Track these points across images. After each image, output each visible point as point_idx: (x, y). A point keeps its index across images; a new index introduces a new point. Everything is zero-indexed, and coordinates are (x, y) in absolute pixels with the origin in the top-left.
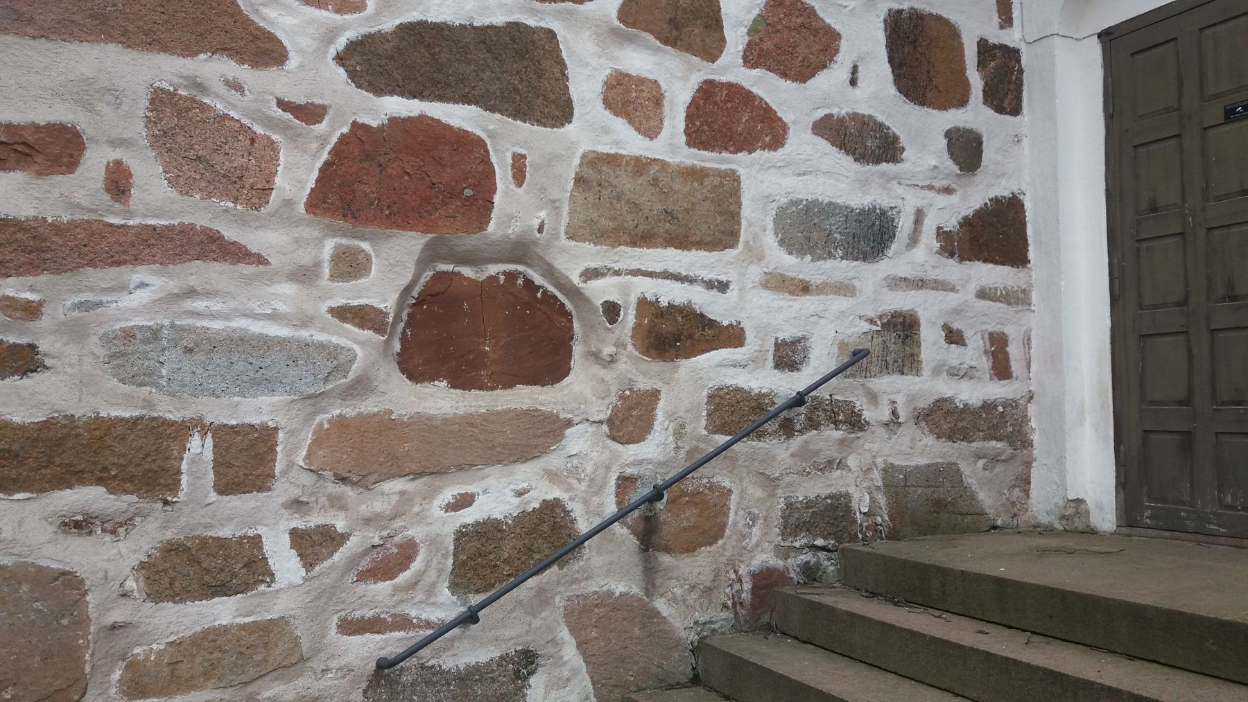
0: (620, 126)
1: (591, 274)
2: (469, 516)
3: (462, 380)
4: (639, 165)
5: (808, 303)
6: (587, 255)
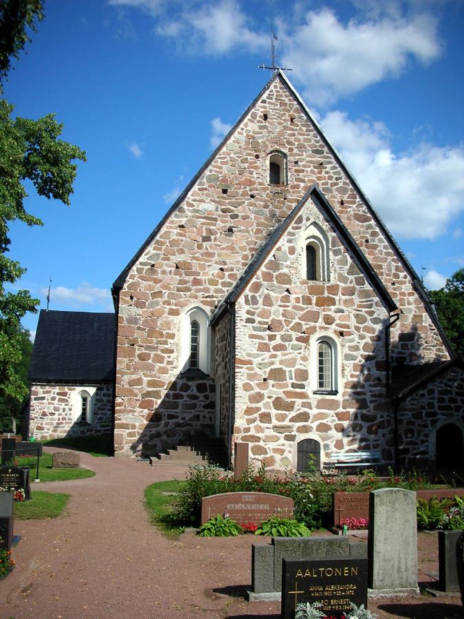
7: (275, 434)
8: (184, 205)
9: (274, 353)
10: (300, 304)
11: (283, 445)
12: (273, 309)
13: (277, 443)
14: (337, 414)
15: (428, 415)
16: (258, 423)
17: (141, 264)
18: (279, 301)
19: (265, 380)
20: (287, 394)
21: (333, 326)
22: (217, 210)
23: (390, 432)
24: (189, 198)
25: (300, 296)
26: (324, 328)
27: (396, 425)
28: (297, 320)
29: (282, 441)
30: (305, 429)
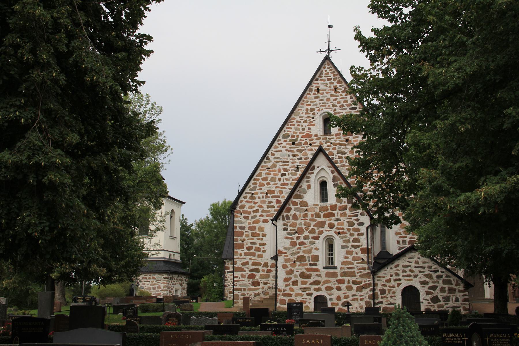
6: (261, 279)
7: (301, 292)
8: (269, 155)
9: (299, 246)
11: (306, 299)
12: (298, 222)
14: (337, 280)
15: (395, 280)
16: (291, 286)
17: (246, 193)
18: (302, 217)
19: (294, 262)
20: (307, 269)
21: (334, 229)
22: (289, 155)
23: (370, 291)
25: (313, 213)
27: (374, 286)
28: (312, 227)
29: (305, 296)
30: (318, 290)
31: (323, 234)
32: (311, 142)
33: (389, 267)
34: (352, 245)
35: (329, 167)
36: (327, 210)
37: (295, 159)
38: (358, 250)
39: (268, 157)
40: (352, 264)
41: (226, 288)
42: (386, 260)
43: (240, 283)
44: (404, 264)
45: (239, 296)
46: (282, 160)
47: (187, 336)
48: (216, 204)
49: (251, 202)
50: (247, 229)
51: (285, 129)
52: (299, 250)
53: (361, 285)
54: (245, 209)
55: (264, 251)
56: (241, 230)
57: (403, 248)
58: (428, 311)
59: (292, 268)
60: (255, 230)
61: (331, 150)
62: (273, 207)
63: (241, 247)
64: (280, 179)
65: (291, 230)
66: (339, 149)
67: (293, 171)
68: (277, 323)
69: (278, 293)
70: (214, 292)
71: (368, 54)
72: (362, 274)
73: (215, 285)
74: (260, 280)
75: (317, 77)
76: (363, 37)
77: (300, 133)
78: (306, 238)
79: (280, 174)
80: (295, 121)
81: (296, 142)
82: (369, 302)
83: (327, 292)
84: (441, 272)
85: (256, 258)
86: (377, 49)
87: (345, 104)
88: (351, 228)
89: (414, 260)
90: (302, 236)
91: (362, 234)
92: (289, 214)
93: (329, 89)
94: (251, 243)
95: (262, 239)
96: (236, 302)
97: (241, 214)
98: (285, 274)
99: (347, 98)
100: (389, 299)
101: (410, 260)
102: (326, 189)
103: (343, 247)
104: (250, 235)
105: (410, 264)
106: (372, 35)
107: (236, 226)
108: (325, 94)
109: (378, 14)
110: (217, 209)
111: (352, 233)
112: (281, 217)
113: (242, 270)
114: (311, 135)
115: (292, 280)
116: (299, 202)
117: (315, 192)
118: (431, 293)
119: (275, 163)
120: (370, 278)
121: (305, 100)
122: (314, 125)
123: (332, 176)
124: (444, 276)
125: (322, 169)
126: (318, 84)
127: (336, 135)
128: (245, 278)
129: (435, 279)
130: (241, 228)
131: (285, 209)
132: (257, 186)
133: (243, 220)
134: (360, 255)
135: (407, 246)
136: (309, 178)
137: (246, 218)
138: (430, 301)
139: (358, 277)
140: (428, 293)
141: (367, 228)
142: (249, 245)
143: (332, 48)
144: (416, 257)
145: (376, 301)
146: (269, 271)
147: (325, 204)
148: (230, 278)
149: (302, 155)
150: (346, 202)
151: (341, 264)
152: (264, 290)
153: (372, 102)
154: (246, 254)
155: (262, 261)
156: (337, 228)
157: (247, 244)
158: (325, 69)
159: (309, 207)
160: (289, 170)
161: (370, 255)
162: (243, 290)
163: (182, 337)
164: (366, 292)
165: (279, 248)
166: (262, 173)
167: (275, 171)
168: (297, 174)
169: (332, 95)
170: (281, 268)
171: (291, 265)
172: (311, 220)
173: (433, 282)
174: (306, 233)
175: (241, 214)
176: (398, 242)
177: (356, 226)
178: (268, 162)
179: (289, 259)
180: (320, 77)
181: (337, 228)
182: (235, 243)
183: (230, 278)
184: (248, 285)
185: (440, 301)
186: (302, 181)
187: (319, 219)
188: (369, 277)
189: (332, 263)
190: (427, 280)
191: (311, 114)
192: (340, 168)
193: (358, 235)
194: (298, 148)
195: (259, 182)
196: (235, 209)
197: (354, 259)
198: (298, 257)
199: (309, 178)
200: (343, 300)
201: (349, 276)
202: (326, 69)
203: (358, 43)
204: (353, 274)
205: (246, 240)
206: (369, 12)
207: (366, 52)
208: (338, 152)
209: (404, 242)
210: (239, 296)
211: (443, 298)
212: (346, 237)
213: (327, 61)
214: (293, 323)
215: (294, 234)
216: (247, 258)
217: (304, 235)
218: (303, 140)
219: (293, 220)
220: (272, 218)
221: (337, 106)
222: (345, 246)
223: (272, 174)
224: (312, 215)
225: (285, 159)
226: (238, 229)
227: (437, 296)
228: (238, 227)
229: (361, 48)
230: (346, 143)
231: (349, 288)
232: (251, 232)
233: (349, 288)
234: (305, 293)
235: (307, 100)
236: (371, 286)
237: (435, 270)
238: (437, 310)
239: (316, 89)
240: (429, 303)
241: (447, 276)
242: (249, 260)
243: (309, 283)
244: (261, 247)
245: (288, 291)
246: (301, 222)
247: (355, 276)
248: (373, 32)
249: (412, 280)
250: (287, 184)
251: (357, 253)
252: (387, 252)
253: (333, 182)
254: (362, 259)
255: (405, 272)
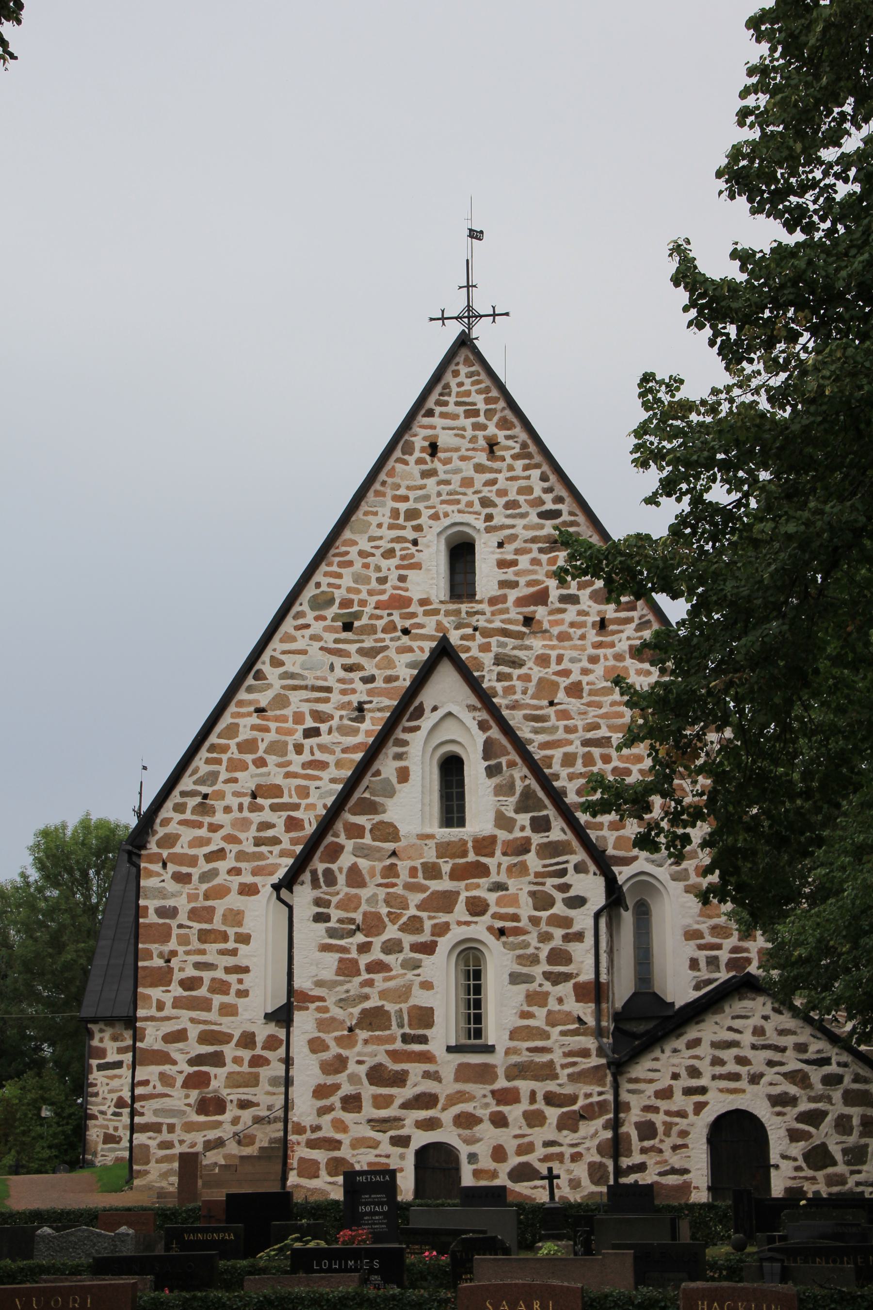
0: (235, 1066)
1: (228, 1094)
2: (205, 1139)
3: (207, 1115)
4: (239, 1073)
5: (275, 1097)
6: (228, 1091)
8: (264, 665)
9: (367, 976)
10: (420, 879)
11: (388, 1156)
12: (365, 893)
13: (377, 1152)
14: (493, 1092)
15: (689, 1091)
16: (339, 1113)
17: (183, 794)
18: (378, 876)
19: (351, 1030)
20: (394, 1055)
21: (486, 919)
22: (332, 668)
23: (605, 1127)
24: (275, 650)
25: (417, 863)
26: (467, 923)
27: (617, 1112)
28: (413, 911)
29: (386, 1147)
30: (431, 1124)
31: (449, 936)
32: (407, 623)
33: (668, 1048)
34: (544, 973)
35: (472, 708)
36: (464, 854)
37: (352, 681)
38: (566, 989)
39: (259, 672)
40: (547, 1036)
41: (91, 1123)
42: (650, 1025)
43: (156, 1104)
44: (716, 1038)
45: (152, 1150)
46: (310, 682)
47: (75, 1301)
48: (56, 829)
49: (200, 825)
50: (182, 918)
51: (318, 577)
52: (366, 990)
53: (575, 1107)
54: (177, 849)
55: (243, 994)
56: (161, 921)
57: (709, 982)
58: (794, 1194)
59: (341, 1051)
60: (210, 921)
61: (475, 652)
62: (276, 841)
63: (163, 977)
64: (299, 749)
65: (340, 921)
66: (500, 650)
67: (346, 722)
68: (323, 1244)
69: (292, 1138)
70: (41, 1137)
71: (717, 334)
72: (576, 1069)
73: (46, 1113)
74: (224, 1092)
75: (430, 403)
76: (702, 279)
77: (371, 593)
78: (391, 947)
79: (300, 728)
80: (354, 551)
81: (357, 624)
82: (602, 1165)
83: (461, 1131)
84: (839, 1064)
85: (213, 1015)
86: (744, 321)
87: (521, 499)
88: (544, 914)
89: (751, 1022)
90: (378, 942)
91: (579, 937)
92: (334, 867)
93: (471, 446)
94: (197, 966)
95: (234, 952)
96: (139, 1171)
97: (165, 865)
98: (318, 1071)
99: (528, 478)
100: (668, 1153)
101: (737, 1024)
102: (461, 784)
103: (515, 979)
104: (194, 939)
105: (736, 1037)
106: (734, 272)
107: (146, 908)
108: (456, 463)
109: (750, 200)
110: (57, 847)
111: (547, 933)
112: (307, 876)
113: (164, 1058)
114: (408, 602)
115: (341, 1093)
116: (368, 827)
117: (423, 792)
118: (806, 1136)
119: (283, 692)
120: (604, 1085)
121: (390, 480)
122: (417, 566)
123: (480, 738)
124: (847, 1080)
125: (450, 714)
126: (433, 427)
127: (493, 601)
128: (172, 1086)
129: (819, 1087)
130: (162, 912)
131: (321, 849)
132: (222, 768)
133: (171, 886)
134: (573, 1007)
135: (723, 975)
136: (405, 743)
137: (182, 878)
138: (801, 1162)
139: (563, 1079)
140: (794, 1136)
141: (597, 916)
142: (191, 972)
143: (481, 307)
144: (758, 1015)
145: (625, 1162)
146: (258, 1061)
147: (454, 834)
148: (106, 1089)
149: (378, 667)
150: (528, 829)
151: (507, 1037)
152: (239, 1128)
153: (708, 497)
154: (178, 1003)
155: (233, 1026)
156: (496, 916)
157: (181, 969)
158: (458, 380)
159: (402, 843)
160: (332, 717)
161: (604, 1006)
162: (165, 1128)
163: (57, 1302)
164: (592, 1130)
165: (297, 984)
166: (237, 725)
167: (284, 719)
168: (359, 728)
169: (479, 468)
170: (306, 1050)
171: (339, 1040)
172: (408, 887)
173: (811, 1099)
174: (392, 932)
175: (165, 865)
176: (694, 964)
177: (559, 909)
178: (261, 690)
179: (333, 1019)
180: (439, 403)
181: (495, 916)
182: (140, 964)
183: (106, 1089)
184: (184, 1113)
185: (834, 1163)
186: (381, 756)
187: (435, 885)
188: (601, 1082)
189: (478, 1034)
190: (793, 1090)
191: (409, 529)
192: (505, 713)
193: (567, 938)
194: (362, 641)
195: (229, 755)
196: (144, 847)
197: (552, 1020)
198: (364, 1012)
199: (405, 743)
200: (514, 1160)
201: (536, 1078)
202: (462, 378)
203: (682, 296)
204: (547, 1072)
205: (181, 956)
206: (721, 192)
207: (708, 332)
208: (499, 660)
209: (713, 962)
210: (153, 1150)
211: (845, 1151)
212: (527, 945)
213: (464, 353)
214: (364, 1241)
215: (352, 933)
216: (184, 1019)
217: (385, 937)
218: (381, 617)
219: (349, 885)
220: (275, 879)
221: (495, 505)
222: (520, 975)
223: (273, 730)
224: (413, 872)
225: (317, 678)
226: (152, 918)
227: (824, 1146)
228: (151, 911)
229: (693, 313)
230: (524, 629)
231: (534, 1119)
232: (197, 926)
233: (534, 1119)
234: (384, 1138)
235: (396, 480)
236: (607, 1112)
237: (819, 1056)
238: (825, 1191)
239: (426, 444)
240: (798, 1169)
241: (857, 1079)
242: (189, 1026)
243: (398, 1102)
244: (232, 978)
245: (327, 1132)
246: (375, 895)
247: (556, 1077)
248: (737, 263)
249: (744, 1091)
250: (322, 765)
251: (560, 1001)
252: (655, 994)
253: (486, 758)
254: (580, 1020)
255: (721, 1062)
